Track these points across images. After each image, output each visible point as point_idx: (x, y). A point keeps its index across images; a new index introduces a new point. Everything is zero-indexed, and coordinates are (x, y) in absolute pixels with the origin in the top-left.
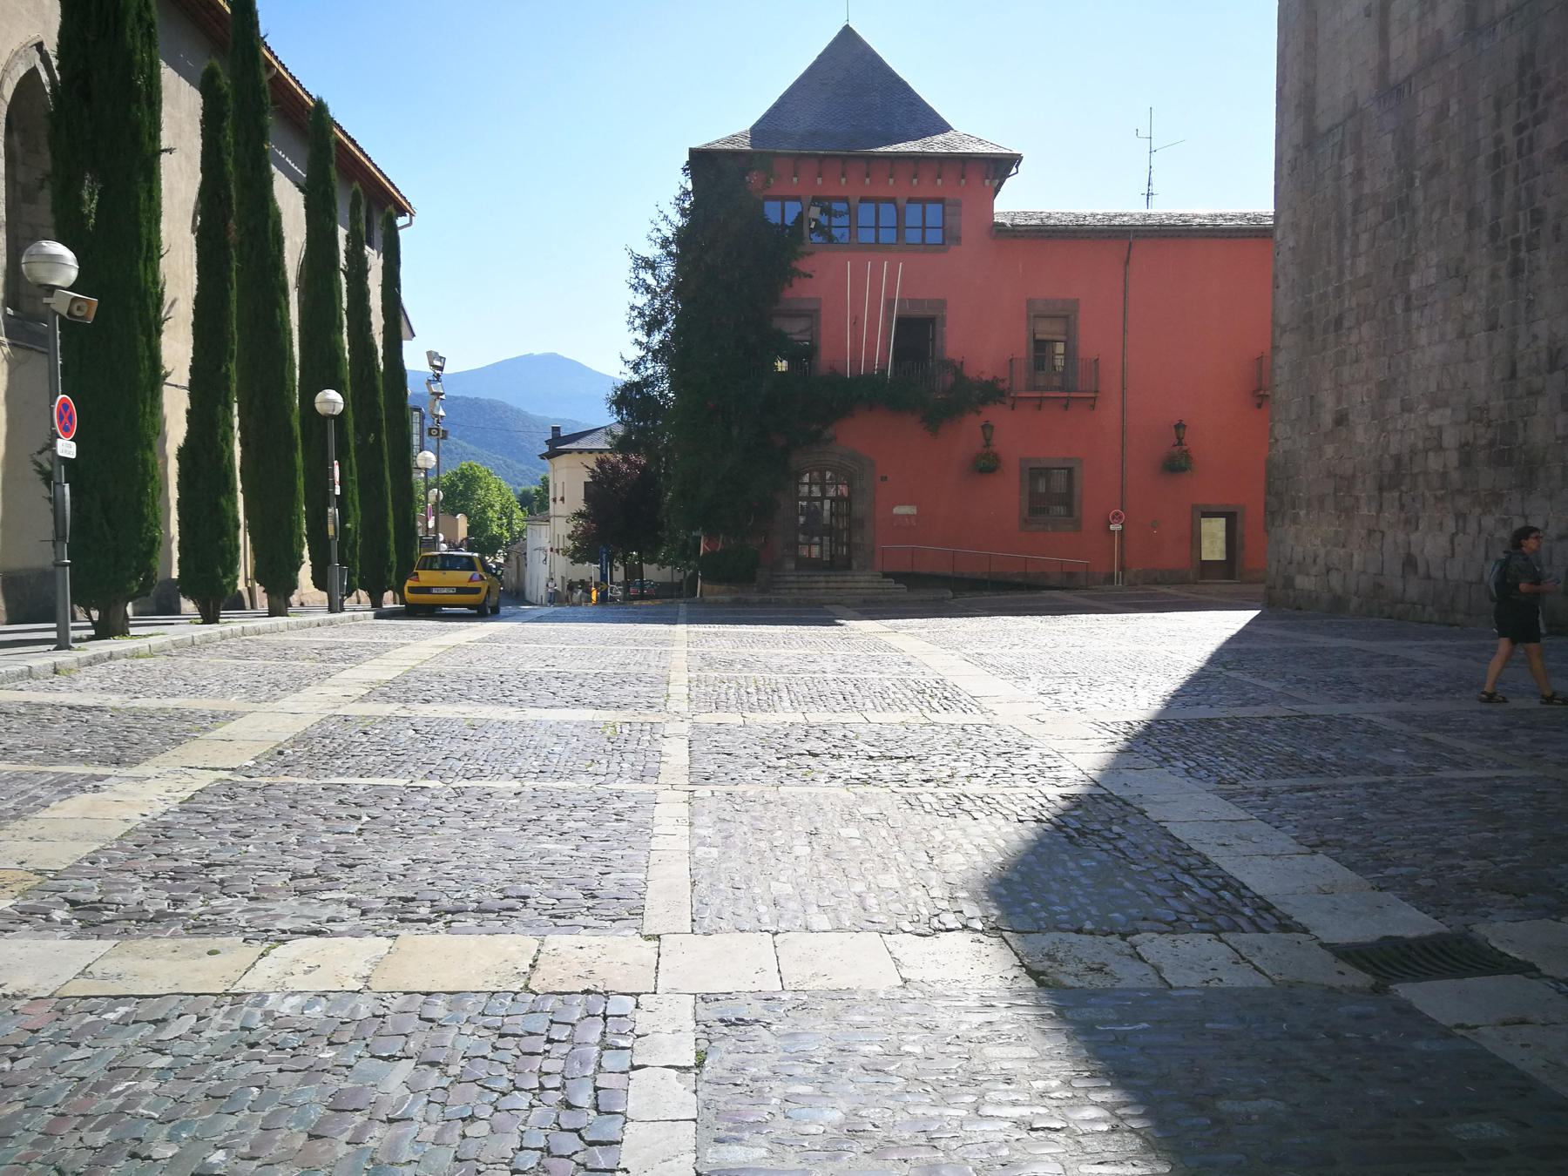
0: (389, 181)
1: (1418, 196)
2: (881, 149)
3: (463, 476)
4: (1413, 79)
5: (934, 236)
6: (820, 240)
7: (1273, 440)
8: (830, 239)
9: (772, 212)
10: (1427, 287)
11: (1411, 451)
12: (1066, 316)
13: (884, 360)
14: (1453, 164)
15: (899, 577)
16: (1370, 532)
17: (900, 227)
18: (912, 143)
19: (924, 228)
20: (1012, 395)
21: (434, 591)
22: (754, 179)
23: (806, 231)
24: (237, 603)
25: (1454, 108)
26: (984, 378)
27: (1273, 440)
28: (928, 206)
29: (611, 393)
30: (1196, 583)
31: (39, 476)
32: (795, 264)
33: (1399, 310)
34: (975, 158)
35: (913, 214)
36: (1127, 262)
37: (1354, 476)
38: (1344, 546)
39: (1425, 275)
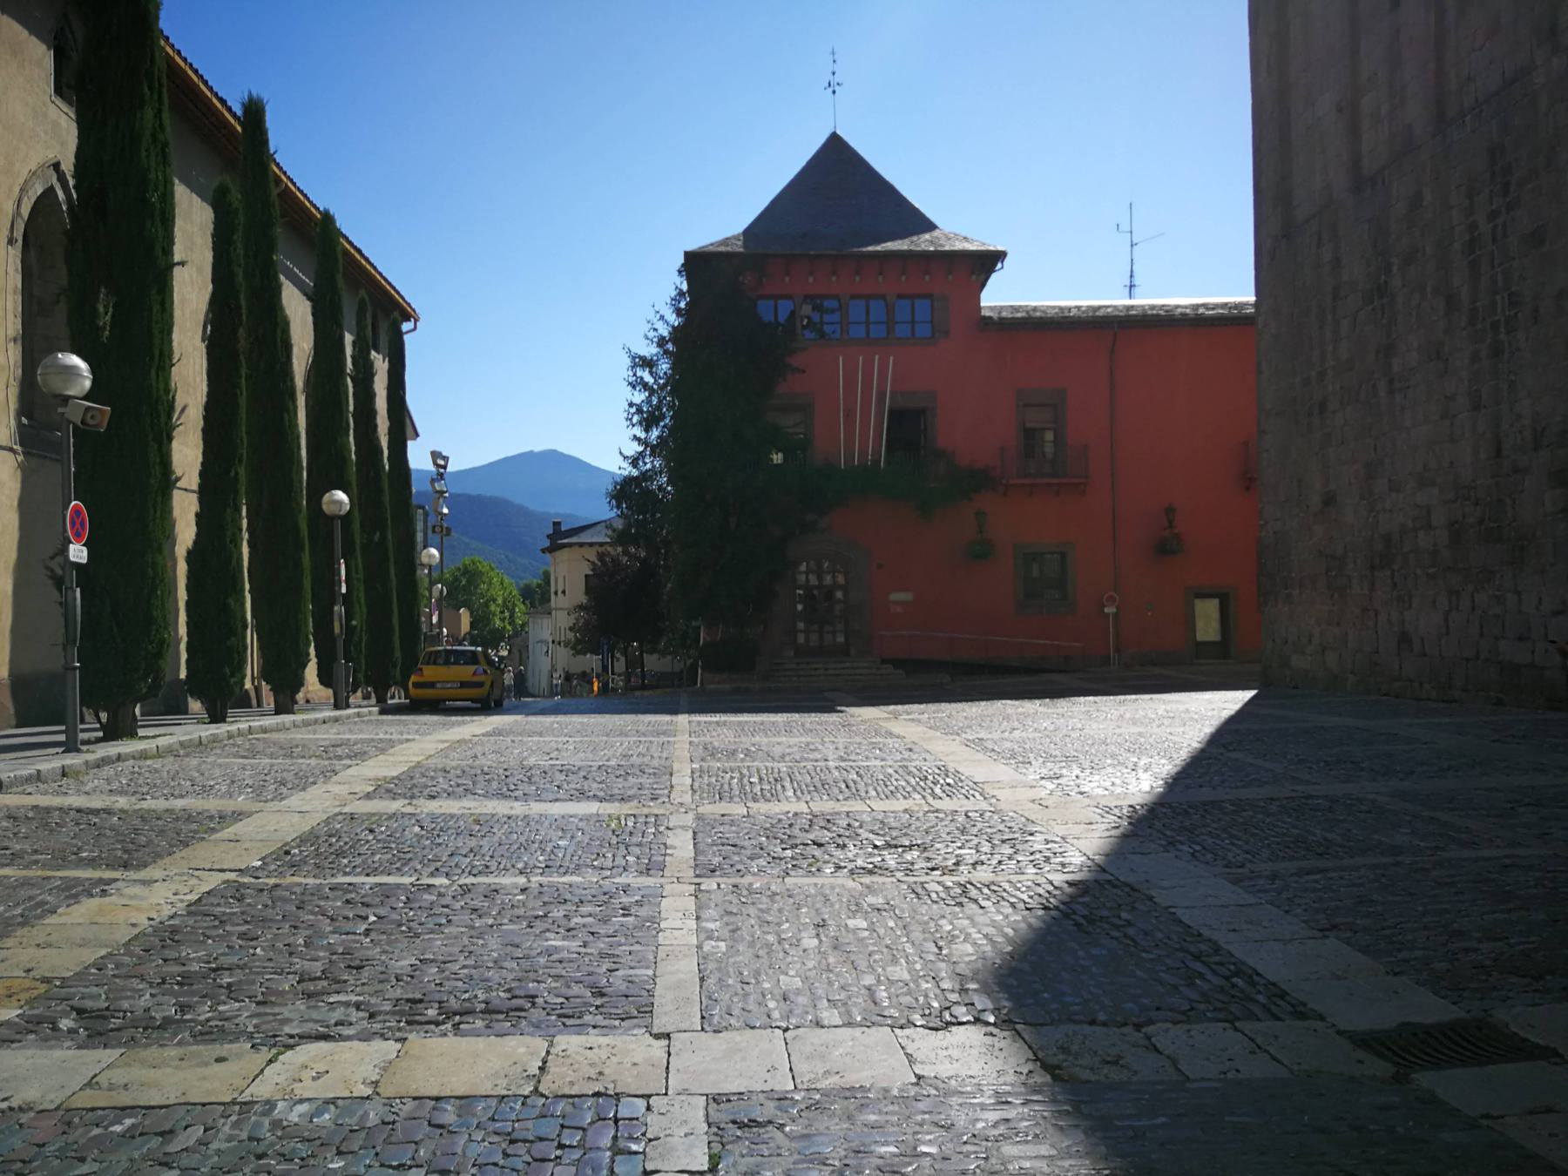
0: (394, 288)
3: (465, 571)
5: (923, 330)
6: (812, 336)
8: (822, 335)
9: (765, 310)
15: (897, 663)
20: (1004, 482)
21: (438, 685)
27: (1262, 522)
29: (610, 488)
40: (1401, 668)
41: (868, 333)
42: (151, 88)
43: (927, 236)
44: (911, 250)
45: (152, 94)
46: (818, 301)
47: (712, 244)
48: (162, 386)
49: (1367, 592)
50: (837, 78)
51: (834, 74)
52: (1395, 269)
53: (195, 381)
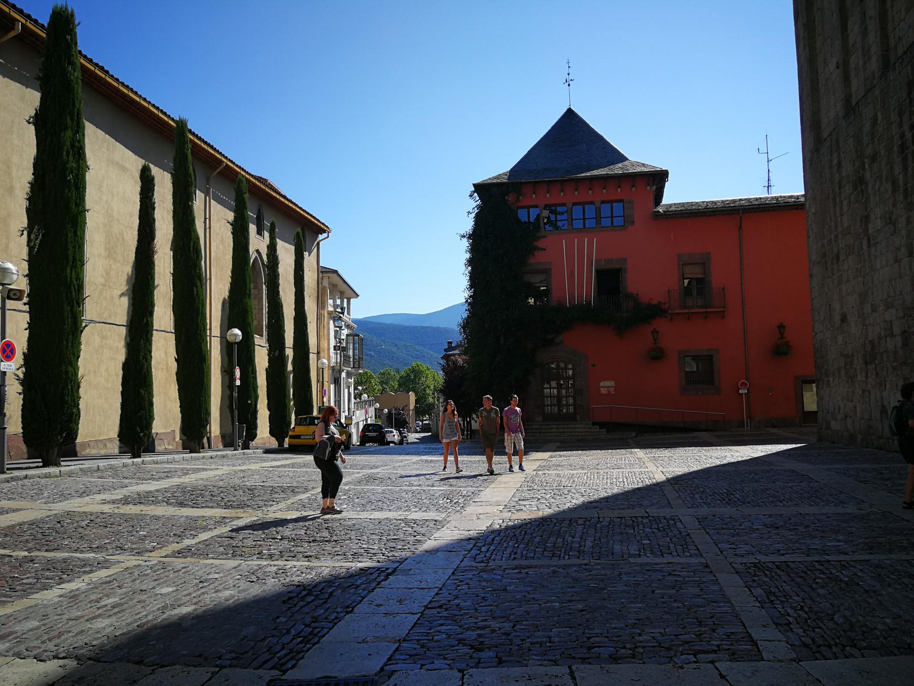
0: (311, 215)
1: (868, 175)
2: (583, 175)
3: (413, 370)
4: (860, 103)
5: (618, 221)
6: (551, 228)
7: (814, 334)
8: (557, 228)
9: (522, 215)
10: (878, 231)
11: (879, 337)
12: (704, 263)
13: (588, 295)
14: (882, 152)
15: (602, 425)
16: (864, 391)
17: (598, 218)
18: (602, 169)
19: (612, 217)
20: (670, 312)
21: (302, 437)
22: (511, 198)
23: (542, 225)
24: (203, 448)
25: (880, 118)
26: (653, 303)
27: (814, 334)
28: (531, 209)
29: (461, 321)
30: (801, 426)
31: (17, 382)
32: (536, 244)
33: (865, 247)
34: (643, 175)
35: (605, 209)
36: (740, 228)
37: (853, 355)
38: (852, 402)
39: (876, 223)
40: (883, 430)
41: (612, 223)
42: (72, 120)
43: (620, 165)
44: (607, 174)
45: (72, 122)
46: (554, 208)
47: (490, 179)
48: (74, 276)
49: (864, 379)
50: (571, 77)
51: (569, 74)
52: (867, 165)
53: (165, 271)
